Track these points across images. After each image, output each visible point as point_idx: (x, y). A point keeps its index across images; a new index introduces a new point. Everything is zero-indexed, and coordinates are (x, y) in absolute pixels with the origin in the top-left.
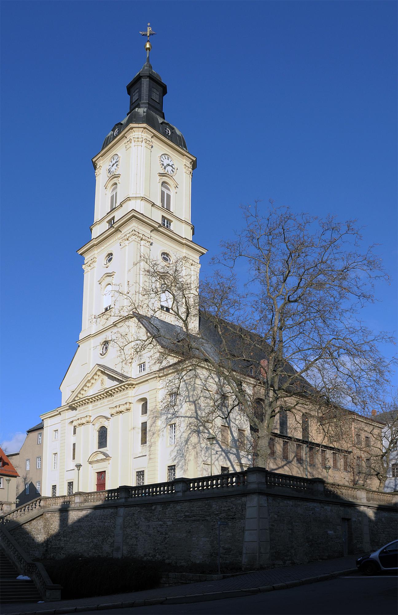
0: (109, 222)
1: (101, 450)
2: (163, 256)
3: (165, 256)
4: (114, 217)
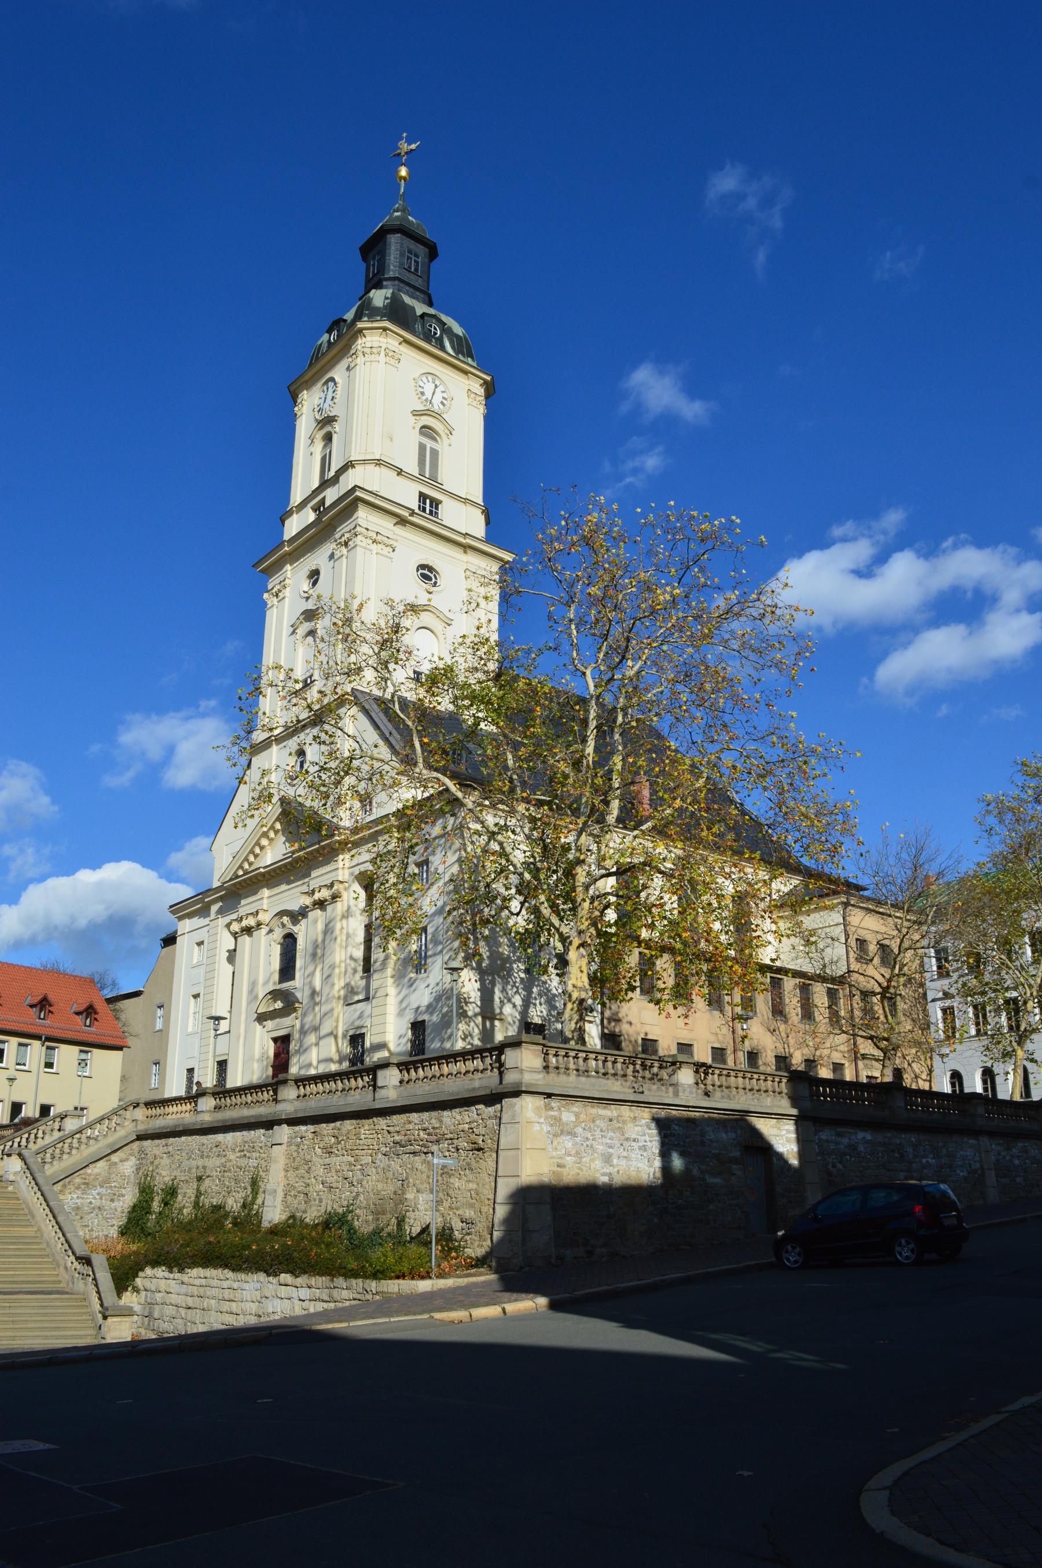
0: (315, 509)
1: (285, 985)
2: (421, 571)
3: (426, 572)
4: (324, 498)
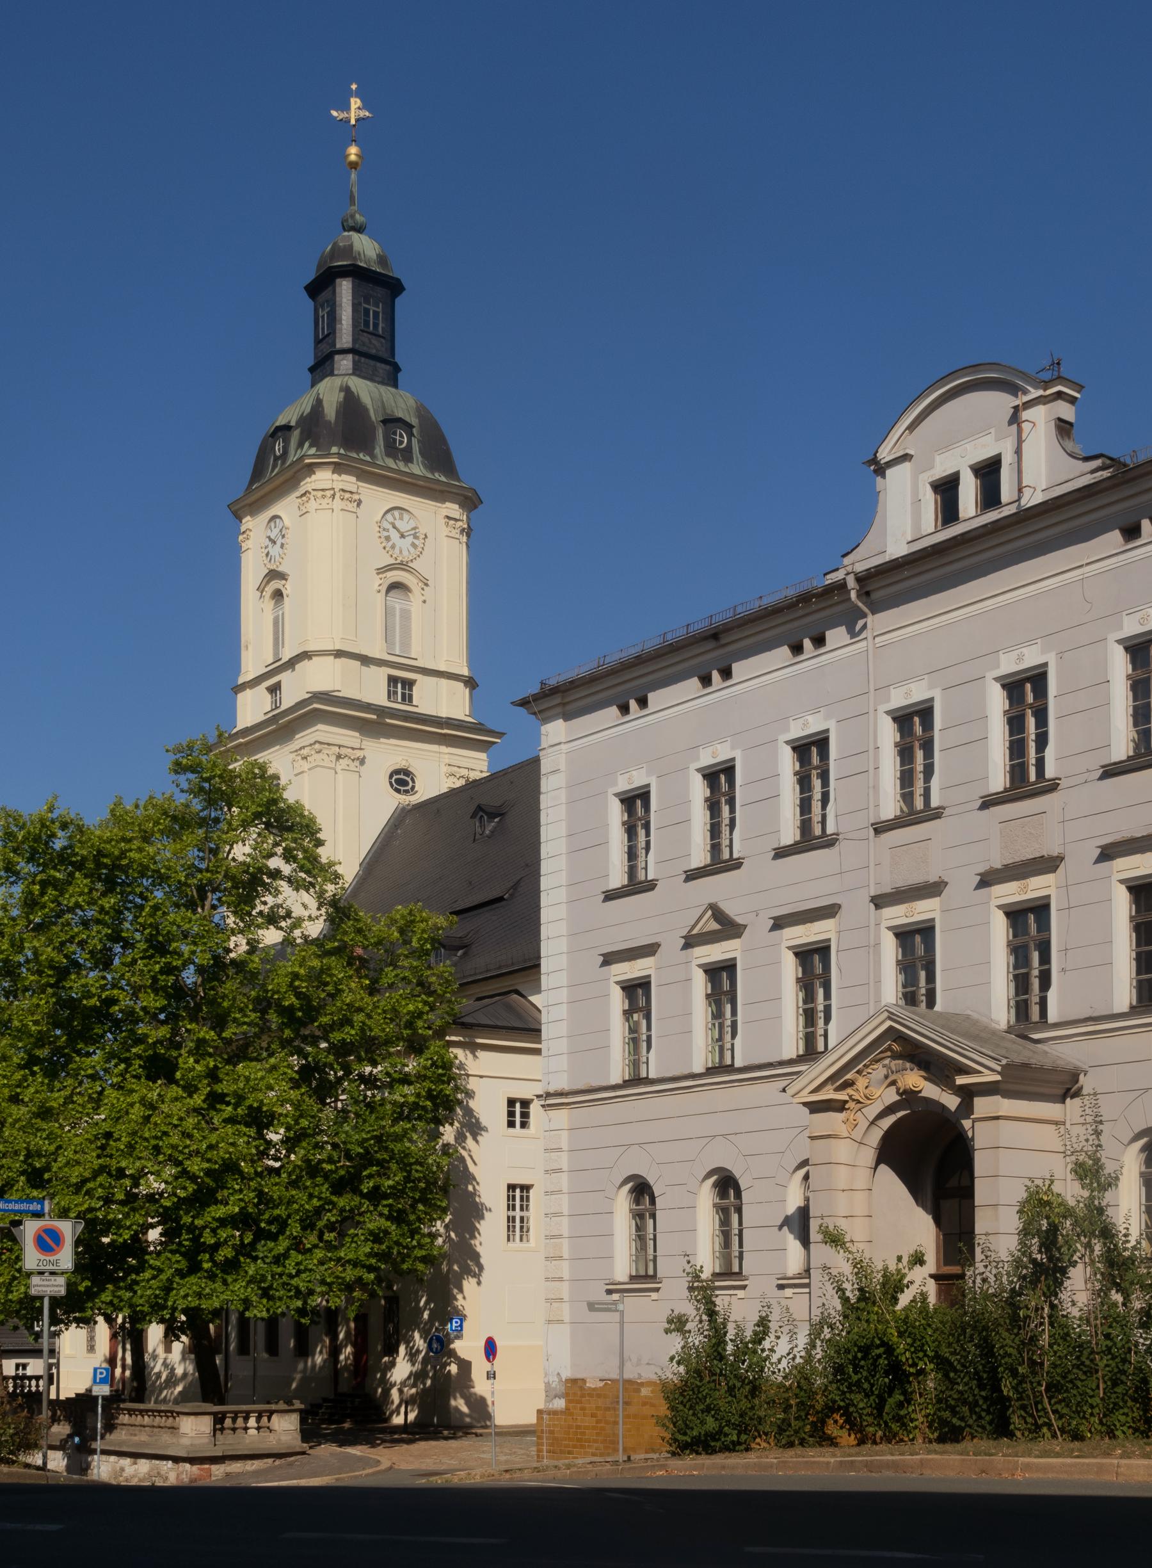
3: (402, 776)
